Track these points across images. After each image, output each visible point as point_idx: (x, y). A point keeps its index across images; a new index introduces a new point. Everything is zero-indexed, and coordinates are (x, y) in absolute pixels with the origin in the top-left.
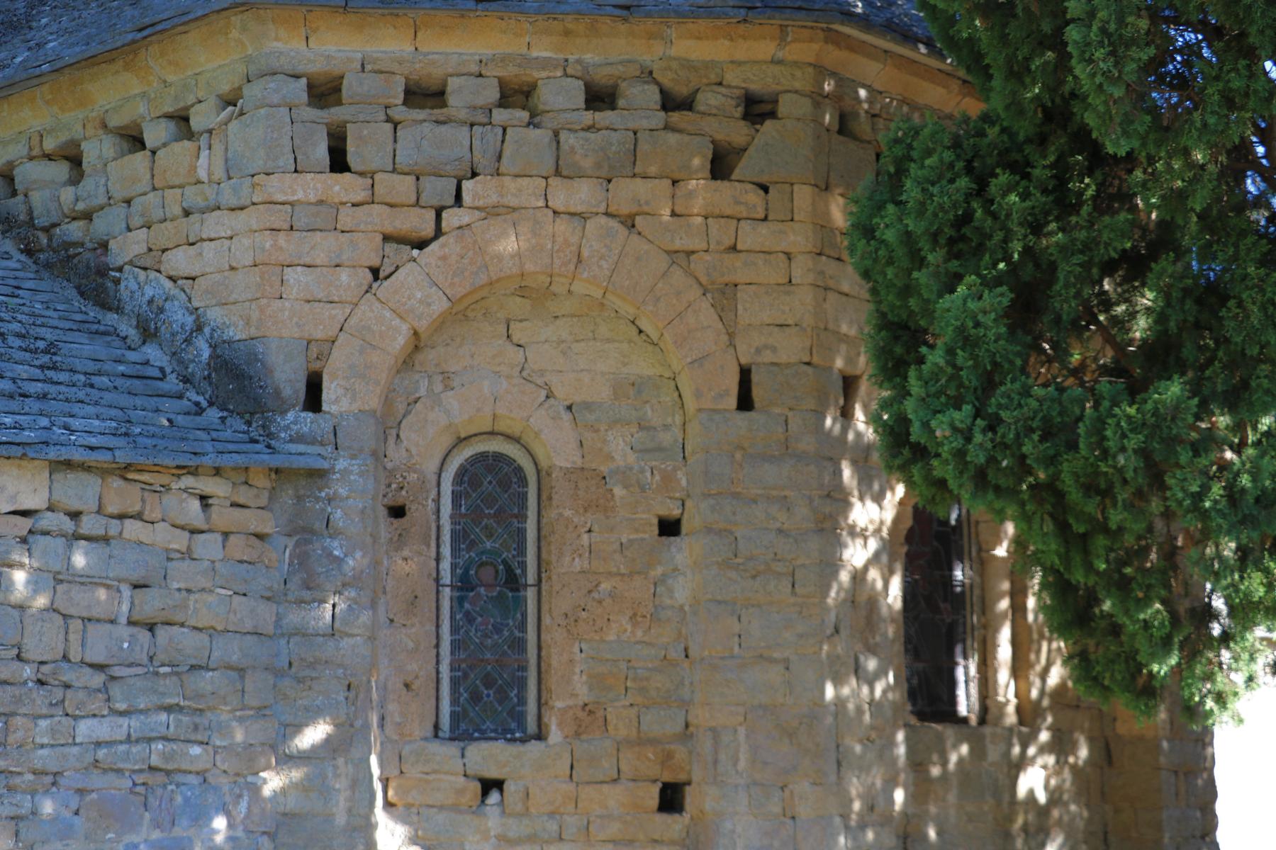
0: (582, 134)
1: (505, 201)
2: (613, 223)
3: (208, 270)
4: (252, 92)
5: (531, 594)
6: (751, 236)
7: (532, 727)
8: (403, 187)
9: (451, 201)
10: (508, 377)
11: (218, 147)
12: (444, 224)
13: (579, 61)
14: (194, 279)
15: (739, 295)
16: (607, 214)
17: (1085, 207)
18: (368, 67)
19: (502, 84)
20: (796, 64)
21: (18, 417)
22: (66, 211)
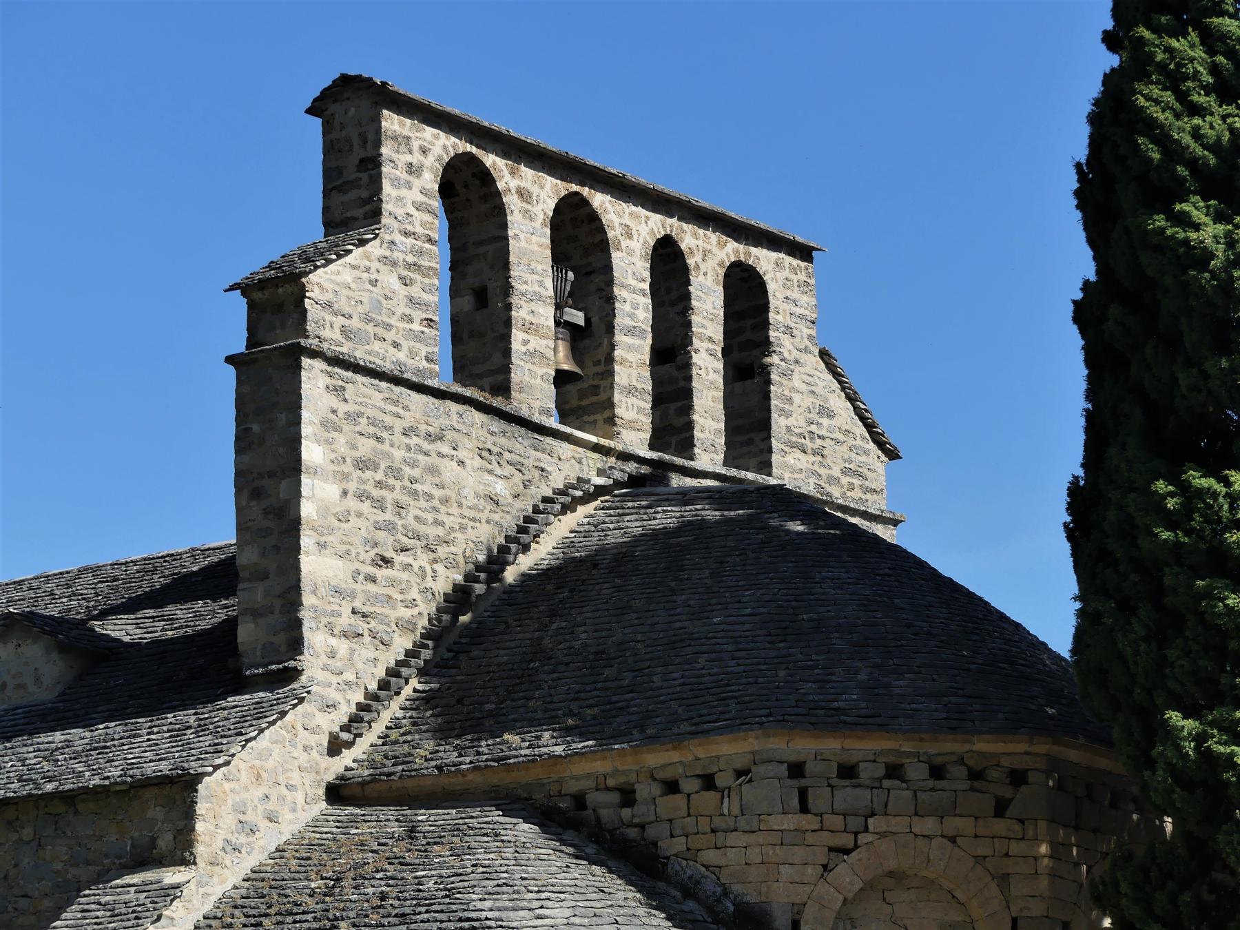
0: (929, 793)
1: (890, 829)
2: (945, 841)
3: (730, 863)
6: (1016, 848)
8: (836, 821)
9: (862, 829)
10: (885, 921)
12: (859, 842)
13: (925, 753)
14: (720, 867)
15: (1011, 880)
16: (942, 836)
17: (1184, 208)
18: (819, 757)
19: (887, 765)
20: (1038, 755)
21: (472, 923)
22: (625, 821)
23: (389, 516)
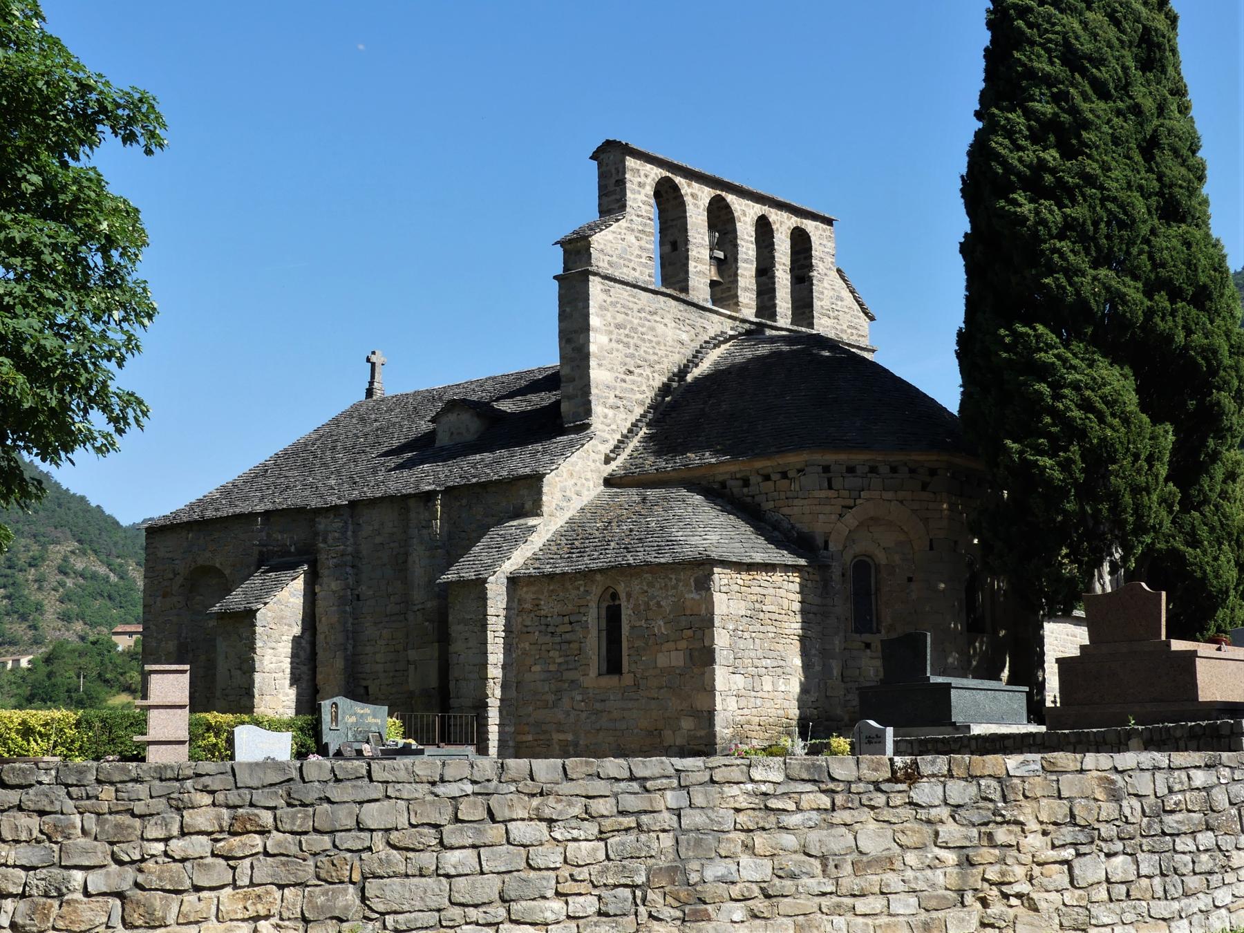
4: (808, 469)
5: (873, 597)
7: (875, 629)
8: (846, 493)
11: (797, 482)
23: (631, 351)
